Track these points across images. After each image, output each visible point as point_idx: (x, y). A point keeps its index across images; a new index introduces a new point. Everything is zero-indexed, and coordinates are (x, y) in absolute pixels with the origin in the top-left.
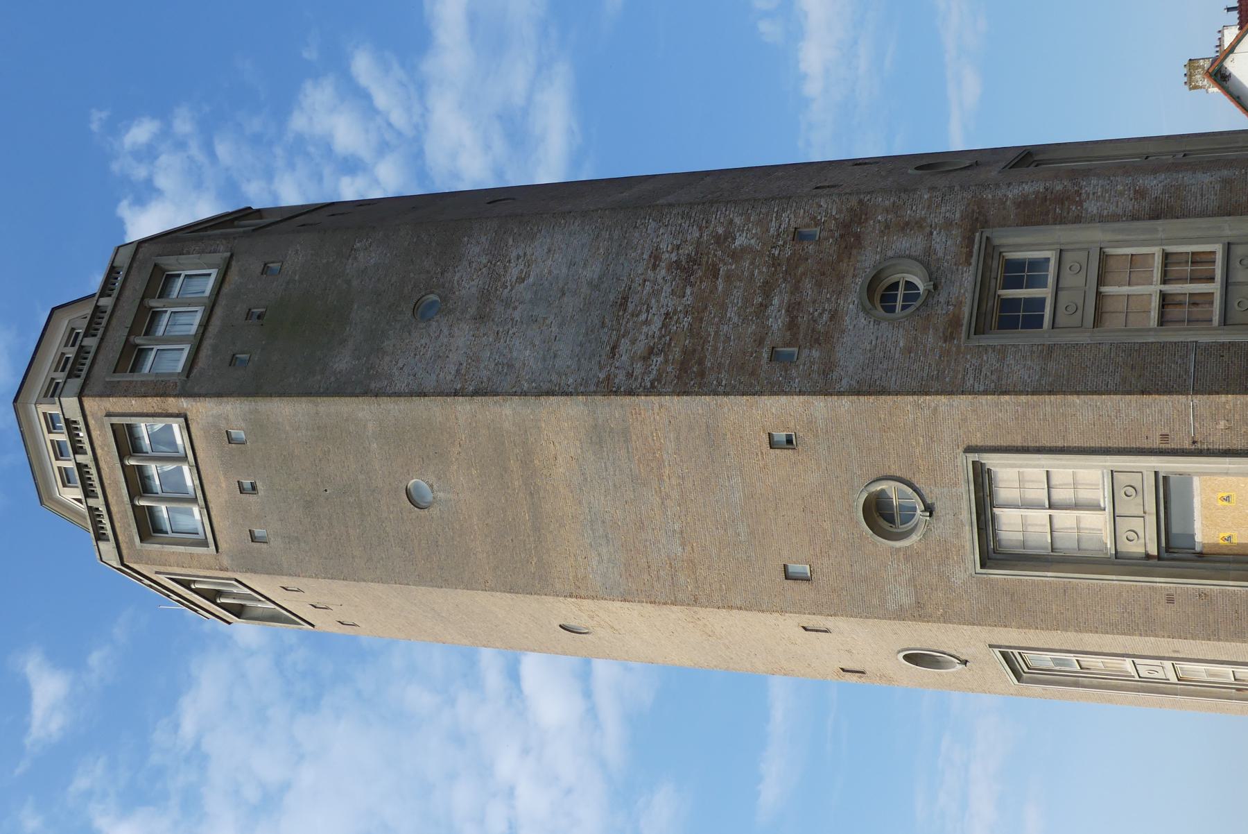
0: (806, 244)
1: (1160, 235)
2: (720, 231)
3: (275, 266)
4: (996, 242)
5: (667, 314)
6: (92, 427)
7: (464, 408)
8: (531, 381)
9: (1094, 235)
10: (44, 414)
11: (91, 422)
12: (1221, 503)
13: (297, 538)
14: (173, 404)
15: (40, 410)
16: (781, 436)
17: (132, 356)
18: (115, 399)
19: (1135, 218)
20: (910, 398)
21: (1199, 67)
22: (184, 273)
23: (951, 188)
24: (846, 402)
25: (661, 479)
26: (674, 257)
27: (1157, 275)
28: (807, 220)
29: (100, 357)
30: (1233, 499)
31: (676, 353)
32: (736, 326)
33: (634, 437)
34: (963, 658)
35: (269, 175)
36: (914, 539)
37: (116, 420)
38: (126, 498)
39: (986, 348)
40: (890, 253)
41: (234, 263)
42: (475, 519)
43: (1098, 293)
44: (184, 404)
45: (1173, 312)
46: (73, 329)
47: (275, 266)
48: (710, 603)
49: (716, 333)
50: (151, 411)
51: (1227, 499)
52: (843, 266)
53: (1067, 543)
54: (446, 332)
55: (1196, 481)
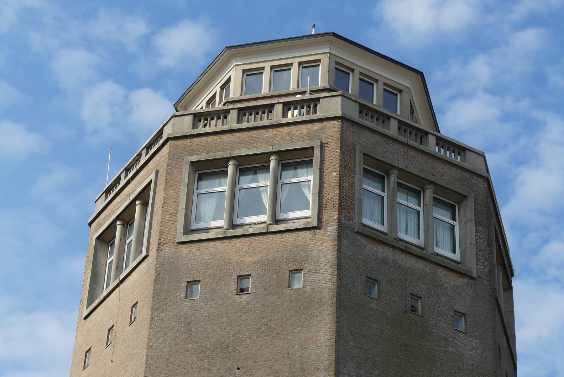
3: (462, 325)
6: (310, 126)
10: (319, 61)
13: (191, 331)
14: (332, 216)
15: (323, 55)
17: (379, 171)
18: (338, 154)
22: (456, 224)
29: (379, 139)
35: (496, 90)
38: (236, 153)
41: (466, 280)
44: (331, 228)
46: (400, 91)
47: (462, 325)
50: (325, 192)
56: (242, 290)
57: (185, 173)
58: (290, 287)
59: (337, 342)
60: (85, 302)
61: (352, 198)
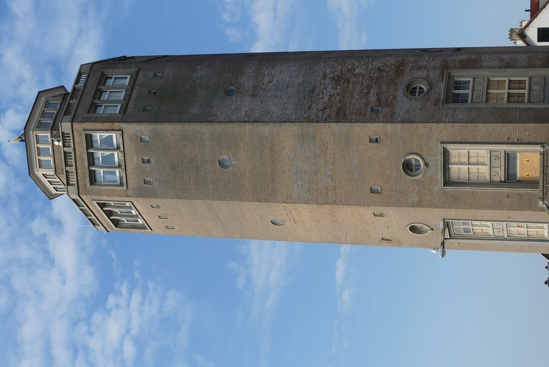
0: (383, 73)
1: (508, 74)
2: (350, 67)
4: (452, 74)
5: (330, 95)
7: (248, 127)
8: (277, 118)
9: (486, 73)
11: (75, 133)
12: (526, 162)
14: (117, 125)
16: (374, 137)
17: (94, 107)
18: (89, 124)
19: (500, 68)
20: (423, 124)
21: (514, 32)
23: (436, 56)
24: (399, 125)
25: (326, 154)
26: (332, 76)
27: (507, 86)
28: (383, 64)
30: (530, 161)
31: (335, 108)
32: (357, 100)
33: (317, 139)
34: (431, 227)
36: (420, 175)
37: (87, 132)
39: (449, 109)
40: (414, 77)
41: (140, 73)
42: (247, 172)
43: (487, 92)
44: (123, 125)
45: (512, 99)
46: (47, 101)
48: (341, 203)
49: (350, 102)
50: (106, 128)
51: (528, 161)
52: (397, 80)
53: (474, 178)
54: (239, 100)
55: (518, 155)
56: (149, 162)
57: (93, 187)
58: (148, 142)
59: (172, 122)
60: (143, 231)
61: (108, 118)
